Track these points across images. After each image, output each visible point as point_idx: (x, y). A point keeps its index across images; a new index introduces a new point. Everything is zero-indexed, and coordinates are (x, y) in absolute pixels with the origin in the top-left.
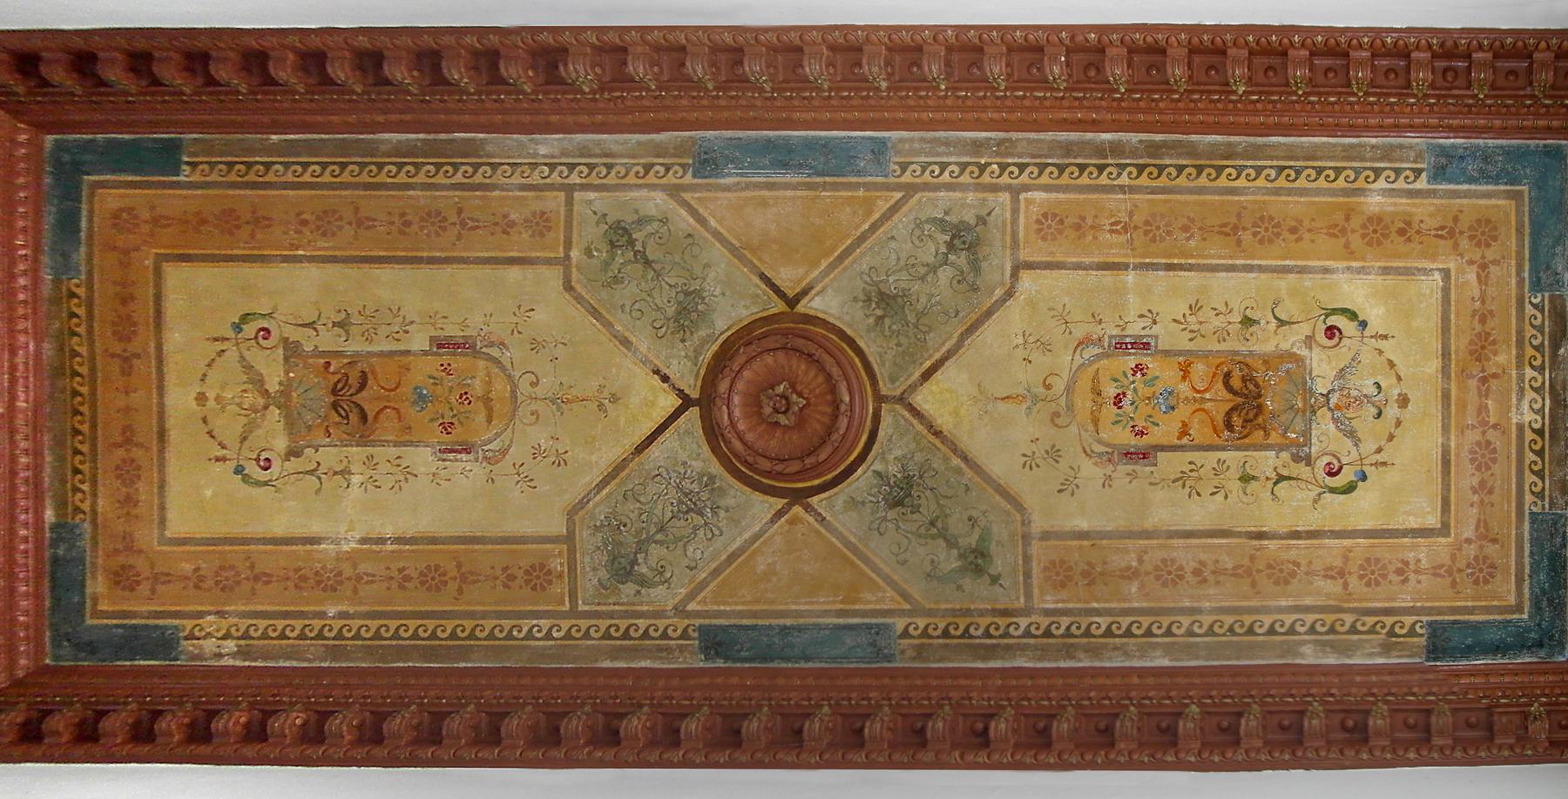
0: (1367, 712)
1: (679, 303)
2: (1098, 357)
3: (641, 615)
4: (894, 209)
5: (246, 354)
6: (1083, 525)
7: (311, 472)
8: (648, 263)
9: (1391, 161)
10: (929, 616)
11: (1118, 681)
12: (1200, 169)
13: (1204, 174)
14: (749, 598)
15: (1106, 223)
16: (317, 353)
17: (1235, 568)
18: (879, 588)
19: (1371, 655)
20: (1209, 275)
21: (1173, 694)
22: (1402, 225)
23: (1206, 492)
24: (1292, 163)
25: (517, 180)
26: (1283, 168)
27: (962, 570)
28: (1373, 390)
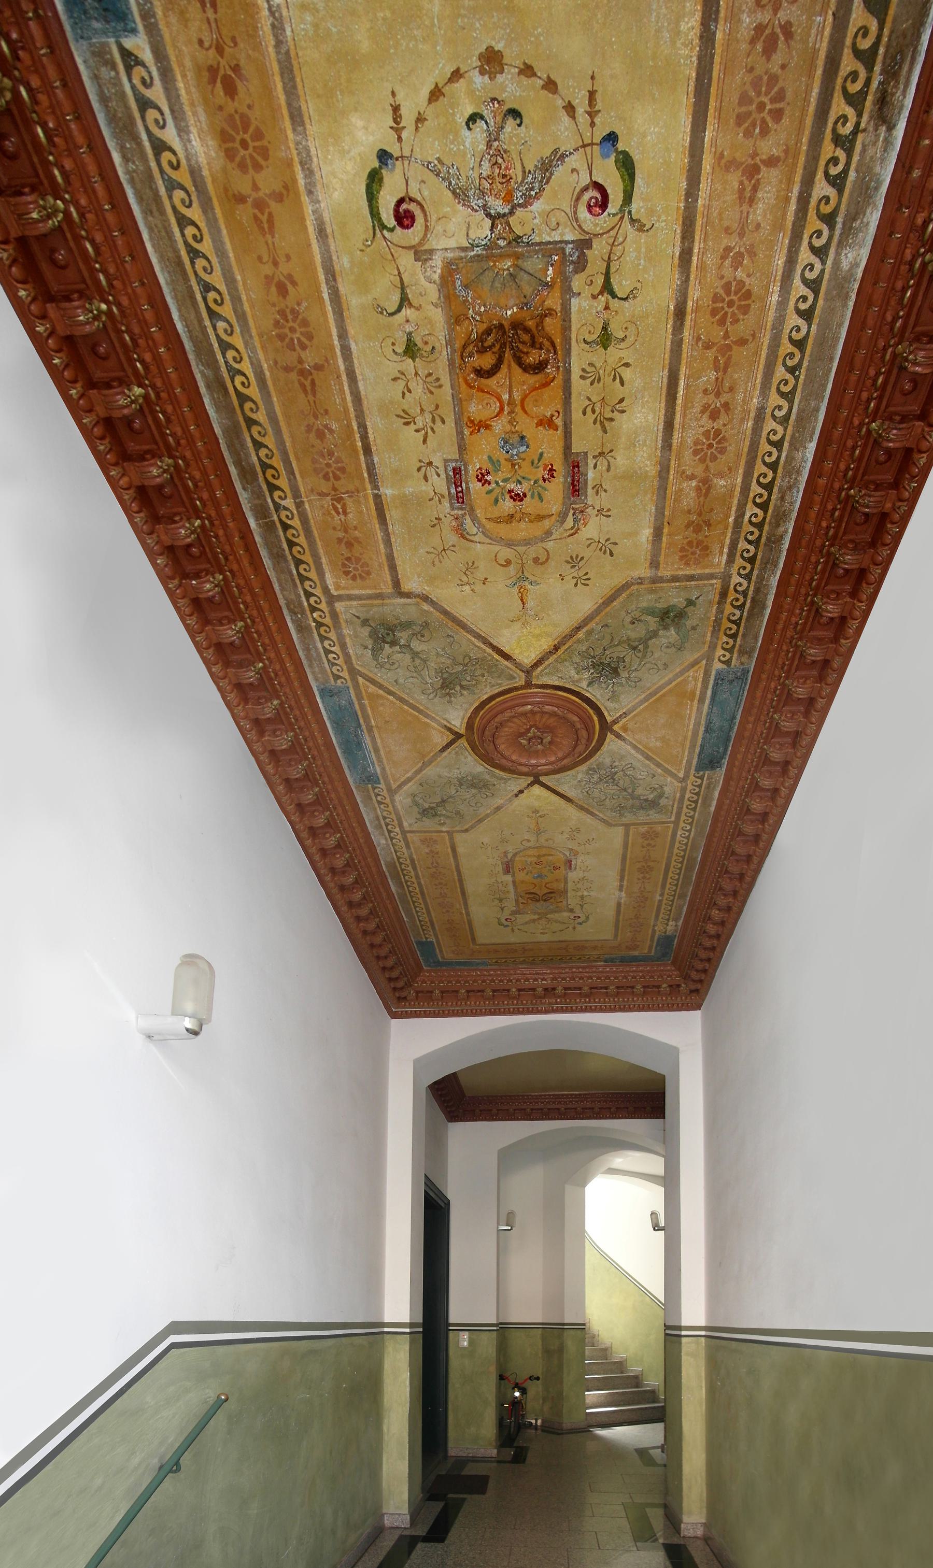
2: (474, 519)
4: (373, 682)
6: (646, 533)
7: (582, 906)
12: (250, 422)
14: (680, 750)
18: (685, 680)
19: (888, 143)
20: (365, 402)
23: (620, 391)
27: (678, 627)
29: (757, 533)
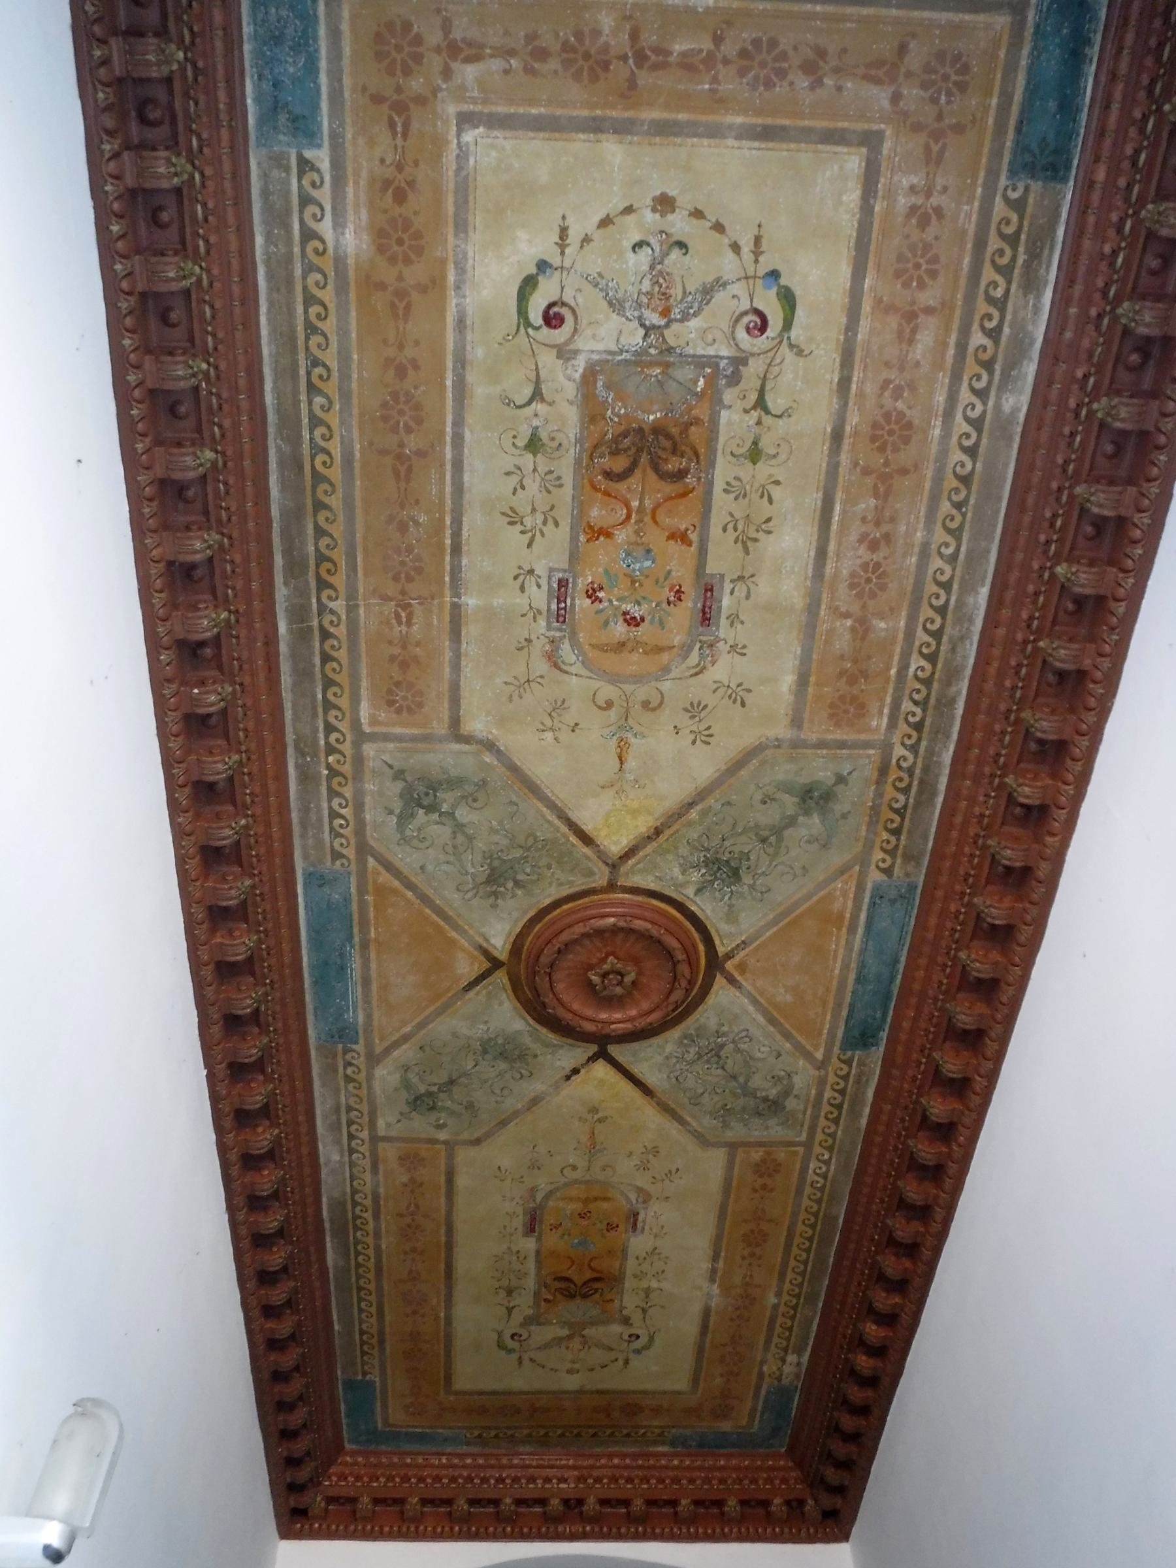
0: (1126, 332)
1: (495, 1059)
2: (574, 643)
3: (820, 1095)
4: (389, 866)
6: (788, 680)
7: (644, 1311)
8: (452, 1082)
9: (288, 212)
10: (872, 847)
11: (996, 652)
12: (319, 506)
13: (326, 500)
14: (819, 1010)
15: (398, 630)
17: (876, 495)
19: (1037, 310)
21: (1031, 588)
22: (391, 372)
23: (766, 510)
24: (302, 372)
25: (368, 1177)
26: (311, 387)
27: (824, 812)
28: (645, 254)
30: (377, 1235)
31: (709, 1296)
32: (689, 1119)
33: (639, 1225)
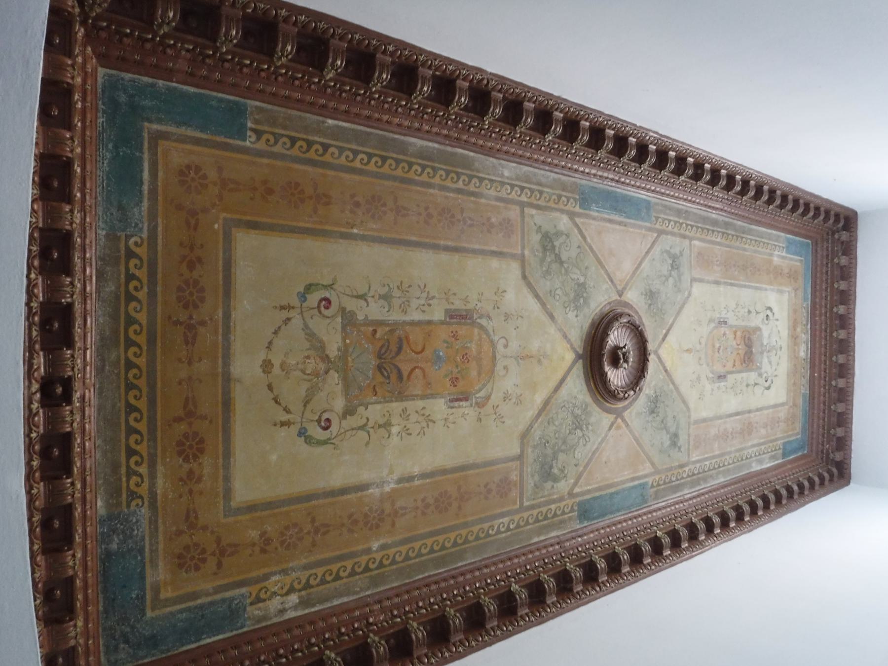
5: (311, 323)
7: (362, 428)
16: (367, 322)
29: (516, 188)
30: (443, 188)
31: (383, 483)
32: (539, 420)
33: (456, 404)
